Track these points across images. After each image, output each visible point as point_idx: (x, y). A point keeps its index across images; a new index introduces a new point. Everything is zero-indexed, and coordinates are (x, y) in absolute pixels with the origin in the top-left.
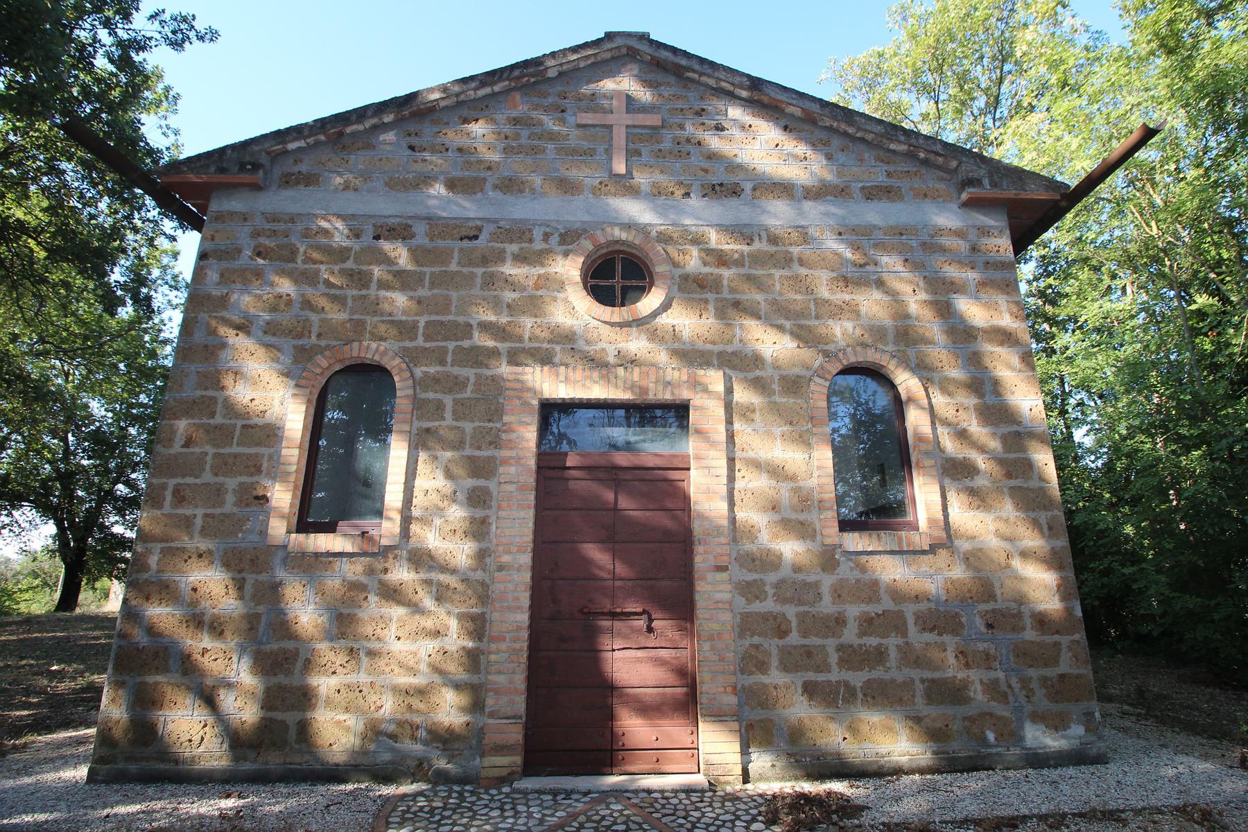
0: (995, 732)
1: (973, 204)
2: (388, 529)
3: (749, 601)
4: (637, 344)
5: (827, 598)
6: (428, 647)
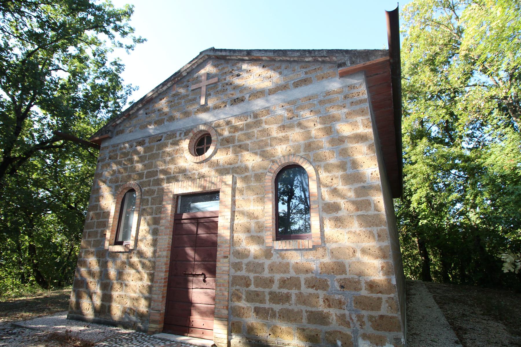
0: (342, 341)
1: (343, 75)
2: (131, 243)
3: (236, 271)
4: (205, 169)
5: (267, 270)
6: (140, 283)
